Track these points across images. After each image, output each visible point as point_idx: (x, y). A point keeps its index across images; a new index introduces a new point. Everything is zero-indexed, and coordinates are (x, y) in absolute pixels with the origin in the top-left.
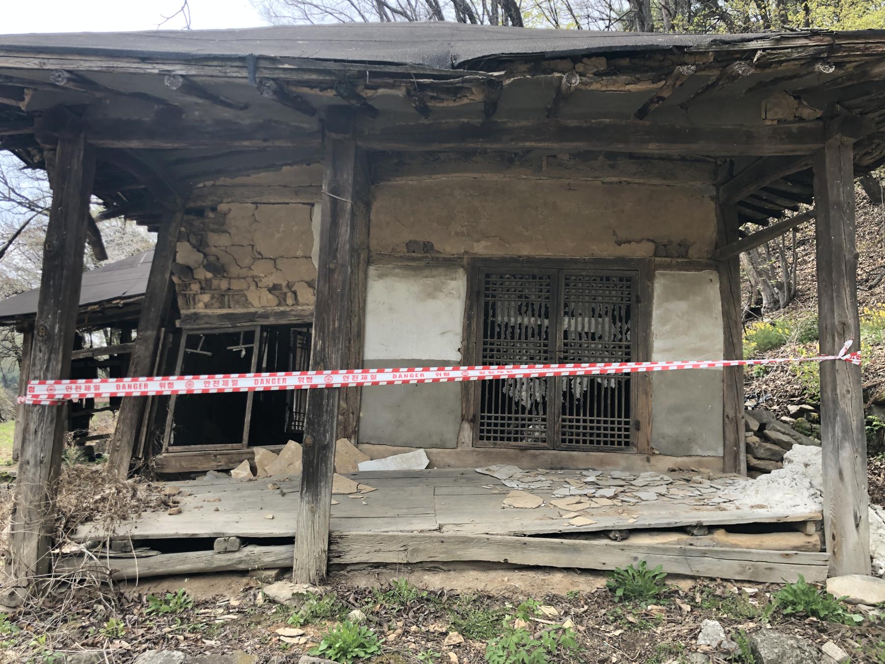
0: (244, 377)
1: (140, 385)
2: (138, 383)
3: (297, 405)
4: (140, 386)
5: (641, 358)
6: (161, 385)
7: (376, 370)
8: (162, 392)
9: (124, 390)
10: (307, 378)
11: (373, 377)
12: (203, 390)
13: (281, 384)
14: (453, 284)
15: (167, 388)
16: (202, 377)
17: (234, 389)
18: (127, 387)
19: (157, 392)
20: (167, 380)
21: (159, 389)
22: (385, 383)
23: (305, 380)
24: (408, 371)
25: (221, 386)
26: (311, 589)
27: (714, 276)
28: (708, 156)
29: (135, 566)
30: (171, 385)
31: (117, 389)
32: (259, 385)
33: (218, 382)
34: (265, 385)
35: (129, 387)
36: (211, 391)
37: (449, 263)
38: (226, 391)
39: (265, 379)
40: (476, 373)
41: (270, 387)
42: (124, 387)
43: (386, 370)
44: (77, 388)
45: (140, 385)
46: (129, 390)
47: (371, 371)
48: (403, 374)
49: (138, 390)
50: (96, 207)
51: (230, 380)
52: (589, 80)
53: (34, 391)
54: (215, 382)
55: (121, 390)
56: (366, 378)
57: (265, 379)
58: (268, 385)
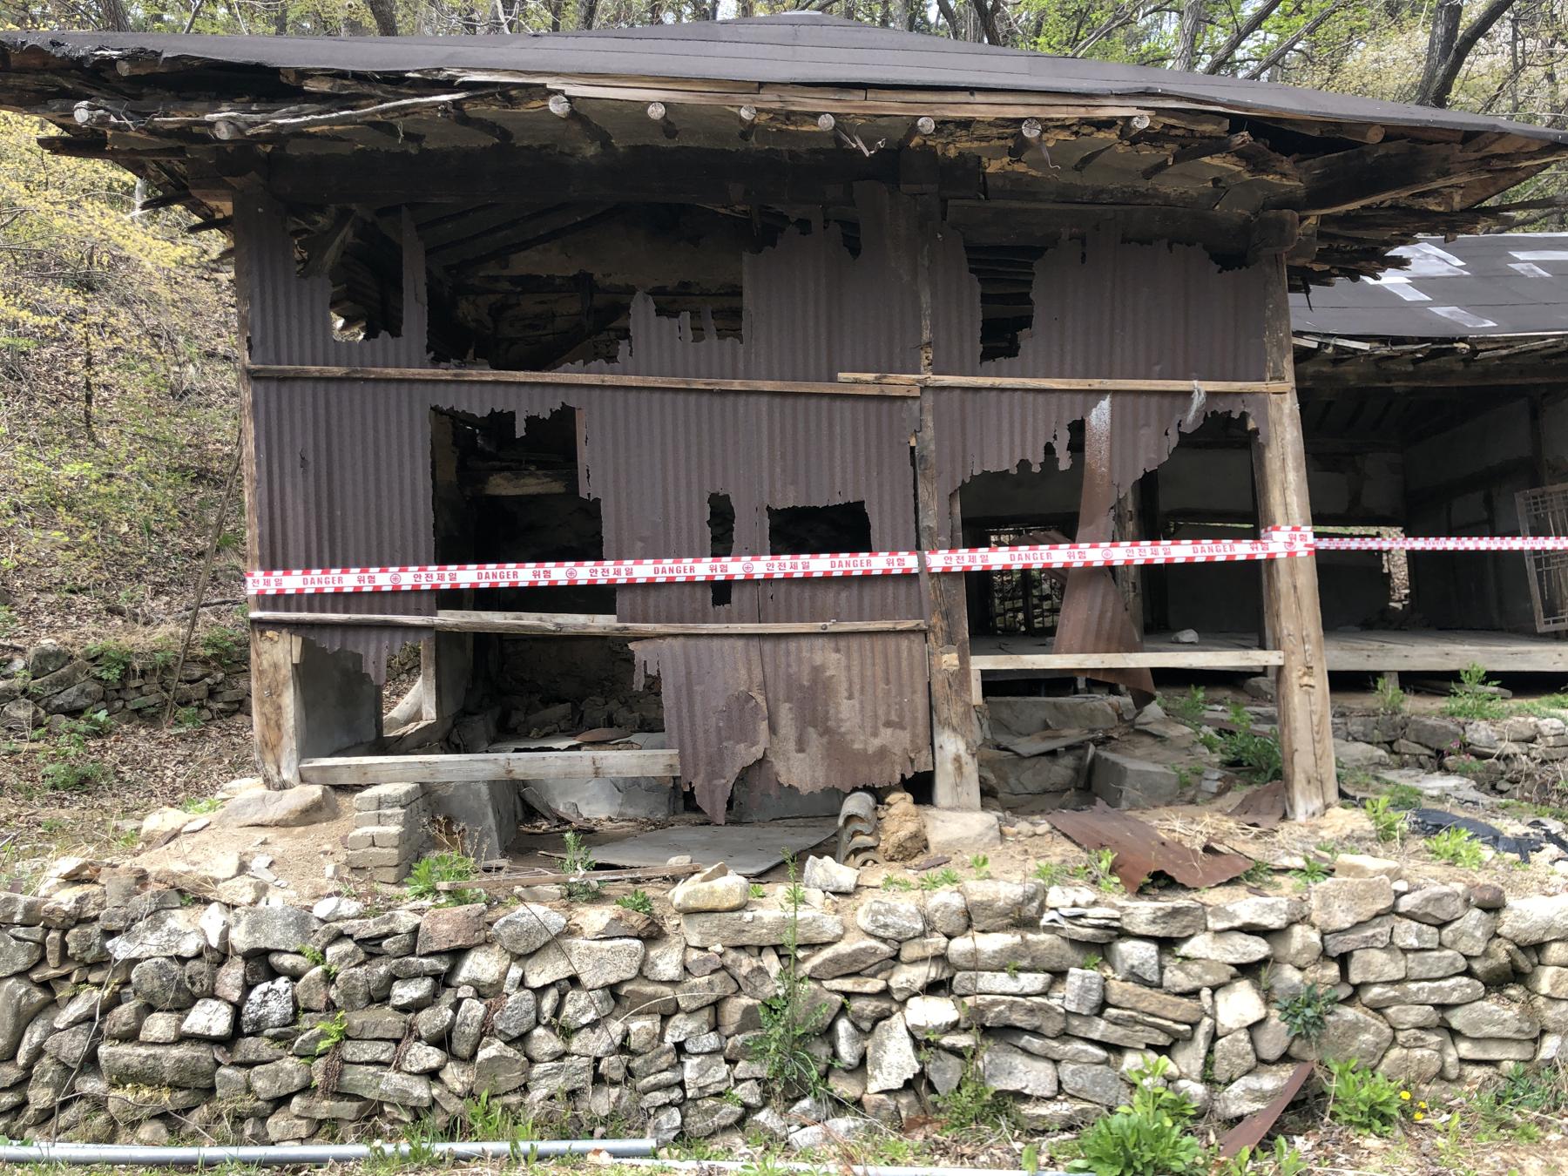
3: (378, 598)
5: (387, 558)
15: (367, 583)
16: (528, 565)
34: (1208, 554)
35: (319, 581)
38: (1156, 562)
39: (1206, 547)
42: (840, 564)
48: (1206, 547)
50: (1370, 281)
52: (774, 123)
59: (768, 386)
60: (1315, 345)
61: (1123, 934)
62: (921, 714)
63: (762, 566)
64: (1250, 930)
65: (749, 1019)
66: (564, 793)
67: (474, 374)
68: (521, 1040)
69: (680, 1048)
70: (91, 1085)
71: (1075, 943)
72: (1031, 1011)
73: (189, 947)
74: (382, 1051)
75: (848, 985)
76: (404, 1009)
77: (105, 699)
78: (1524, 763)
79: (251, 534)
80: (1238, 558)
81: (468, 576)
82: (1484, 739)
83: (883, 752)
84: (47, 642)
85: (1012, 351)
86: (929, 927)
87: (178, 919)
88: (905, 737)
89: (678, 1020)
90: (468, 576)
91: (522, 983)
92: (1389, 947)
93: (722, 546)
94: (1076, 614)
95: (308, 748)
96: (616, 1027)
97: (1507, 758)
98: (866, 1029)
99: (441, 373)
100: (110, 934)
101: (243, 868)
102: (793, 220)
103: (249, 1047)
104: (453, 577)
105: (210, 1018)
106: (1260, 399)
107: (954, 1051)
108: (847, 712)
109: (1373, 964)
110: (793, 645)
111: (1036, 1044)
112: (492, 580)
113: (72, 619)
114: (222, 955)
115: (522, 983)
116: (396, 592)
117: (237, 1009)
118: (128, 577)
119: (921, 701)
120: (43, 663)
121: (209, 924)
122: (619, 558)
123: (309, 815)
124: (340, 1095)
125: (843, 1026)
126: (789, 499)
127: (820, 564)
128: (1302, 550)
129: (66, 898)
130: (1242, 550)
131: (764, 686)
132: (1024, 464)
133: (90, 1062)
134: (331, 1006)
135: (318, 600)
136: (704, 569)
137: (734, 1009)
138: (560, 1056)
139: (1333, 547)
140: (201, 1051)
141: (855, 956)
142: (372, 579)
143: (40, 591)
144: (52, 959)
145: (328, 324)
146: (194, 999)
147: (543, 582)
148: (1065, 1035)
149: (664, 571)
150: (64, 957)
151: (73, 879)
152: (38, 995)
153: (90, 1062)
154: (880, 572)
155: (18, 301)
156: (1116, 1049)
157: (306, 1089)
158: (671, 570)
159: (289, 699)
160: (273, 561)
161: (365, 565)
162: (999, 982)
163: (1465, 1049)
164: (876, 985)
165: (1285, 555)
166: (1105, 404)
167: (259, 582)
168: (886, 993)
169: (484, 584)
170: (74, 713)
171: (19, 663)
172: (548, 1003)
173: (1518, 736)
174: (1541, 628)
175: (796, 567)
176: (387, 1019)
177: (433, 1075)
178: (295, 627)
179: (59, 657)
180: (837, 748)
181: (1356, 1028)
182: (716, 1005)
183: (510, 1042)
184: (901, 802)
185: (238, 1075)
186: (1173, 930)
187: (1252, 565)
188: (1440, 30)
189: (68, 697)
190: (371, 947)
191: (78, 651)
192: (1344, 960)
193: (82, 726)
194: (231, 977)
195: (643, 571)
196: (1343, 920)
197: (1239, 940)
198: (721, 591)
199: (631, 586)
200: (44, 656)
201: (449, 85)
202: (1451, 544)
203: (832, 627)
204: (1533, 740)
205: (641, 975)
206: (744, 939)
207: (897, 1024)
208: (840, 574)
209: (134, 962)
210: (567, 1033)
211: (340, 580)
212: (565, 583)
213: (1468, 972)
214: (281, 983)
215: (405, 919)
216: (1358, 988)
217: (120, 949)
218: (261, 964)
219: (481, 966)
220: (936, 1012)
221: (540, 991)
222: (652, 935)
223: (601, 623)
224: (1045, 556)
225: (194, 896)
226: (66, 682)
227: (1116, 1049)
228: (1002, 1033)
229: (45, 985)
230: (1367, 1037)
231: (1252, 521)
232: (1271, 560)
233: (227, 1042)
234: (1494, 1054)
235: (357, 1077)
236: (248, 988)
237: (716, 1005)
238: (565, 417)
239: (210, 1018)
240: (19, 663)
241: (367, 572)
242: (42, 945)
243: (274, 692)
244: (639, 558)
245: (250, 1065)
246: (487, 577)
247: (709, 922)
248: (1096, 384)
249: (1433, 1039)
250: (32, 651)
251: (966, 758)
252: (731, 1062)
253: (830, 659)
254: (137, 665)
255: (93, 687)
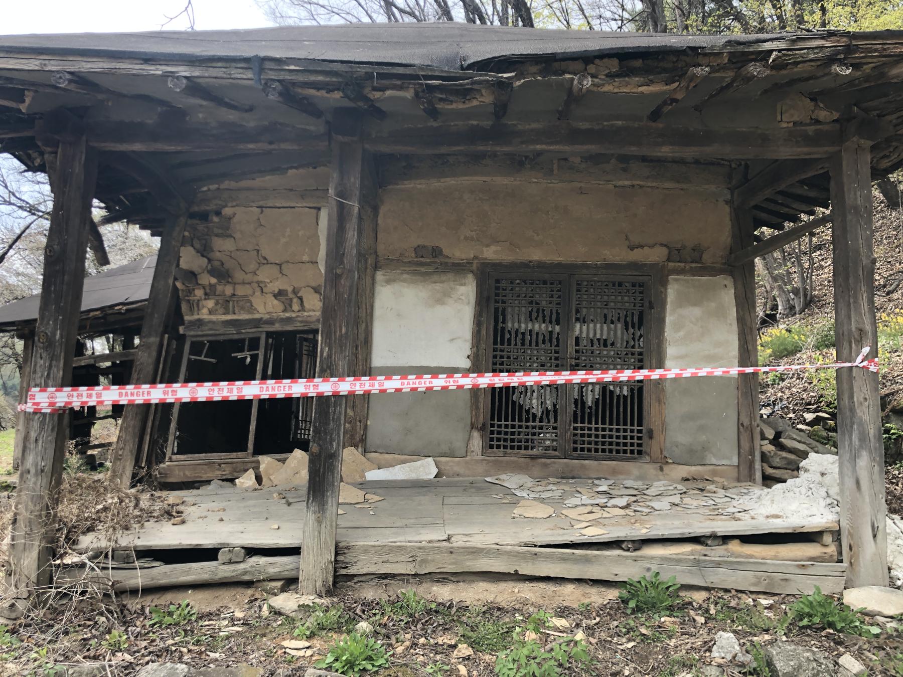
0: (249, 384)
1: (143, 392)
2: (141, 391)
4: (143, 394)
5: (654, 365)
6: (165, 393)
7: (383, 378)
8: (165, 399)
9: (127, 398)
10: (314, 385)
11: (381, 385)
12: (207, 397)
13: (287, 392)
14: (462, 289)
15: (170, 396)
16: (206, 384)
17: (239, 396)
18: (129, 394)
19: (160, 399)
20: (171, 387)
21: (162, 396)
22: (393, 391)
23: (312, 388)
24: (416, 379)
25: (225, 394)
26: (317, 601)
27: (729, 281)
28: (722, 159)
29: (138, 577)
30: (174, 392)
31: (120, 396)
32: (264, 393)
33: (223, 389)
34: (271, 392)
35: (132, 394)
36: (215, 399)
37: (458, 268)
38: (231, 398)
39: (270, 386)
40: (486, 380)
41: (276, 395)
42: (126, 394)
43: (394, 377)
44: (78, 395)
45: (143, 392)
46: (132, 398)
47: (379, 378)
48: (411, 382)
49: (141, 397)
51: (235, 388)
53: (34, 399)
54: (219, 389)
55: (123, 398)
56: (373, 385)
57: (270, 386)
58: (273, 393)
102: (613, 161)
145: (89, 207)
187: (638, 389)
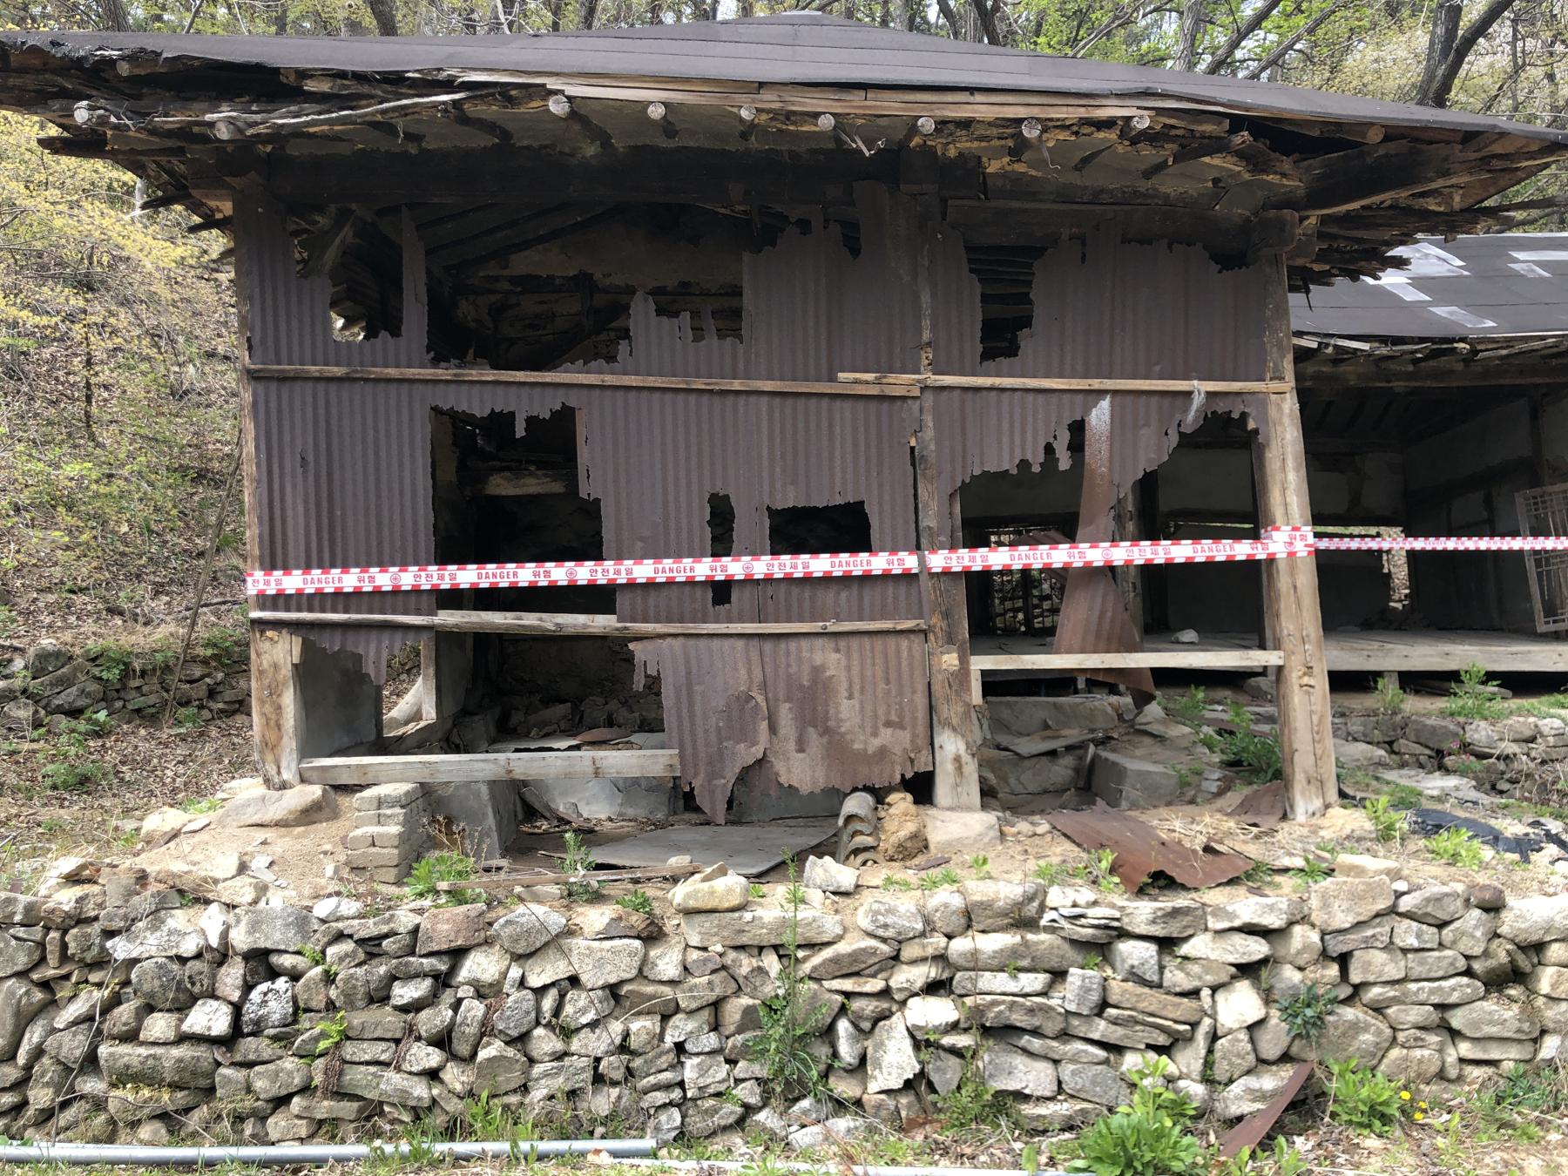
3: (378, 598)
5: (387, 558)
15: (367, 583)
16: (528, 565)
34: (1208, 554)
35: (319, 581)
38: (1156, 562)
39: (1206, 547)
42: (840, 564)
48: (1206, 547)
59: (768, 386)
60: (1315, 345)
61: (1123, 934)
62: (921, 714)
63: (762, 566)
64: (1250, 930)
65: (749, 1019)
66: (564, 793)
67: (474, 374)
68: (521, 1040)
69: (680, 1048)
70: (91, 1085)
71: (1075, 943)
72: (1031, 1011)
73: (189, 947)
74: (382, 1051)
75: (848, 985)
76: (404, 1009)
77: (105, 699)
78: (1524, 763)
79: (251, 534)
80: (1238, 558)
81: (468, 576)
82: (1484, 739)
83: (883, 752)
84: (47, 642)
85: (1012, 351)
86: (929, 927)
87: (178, 919)
88: (905, 737)
89: (678, 1020)
90: (468, 576)
91: (522, 983)
92: (1389, 947)
93: (722, 546)
94: (1076, 614)
95: (308, 748)
96: (616, 1027)
97: (1507, 758)
98: (866, 1029)
99: (441, 373)
100: (110, 934)
101: (243, 868)
102: (793, 220)
103: (249, 1047)
104: (453, 577)
105: (210, 1018)
106: (1260, 399)
107: (954, 1051)
108: (847, 712)
109: (1373, 964)
110: (793, 645)
111: (1036, 1044)
112: (492, 580)
113: (72, 619)
114: (222, 955)
115: (522, 983)
116: (396, 592)
117: (237, 1009)
118: (128, 577)
119: (921, 701)
120: (43, 663)
121: (209, 924)
122: (619, 558)
123: (309, 815)
124: (340, 1095)
125: (843, 1026)
126: (789, 499)
127: (820, 564)
128: (1302, 550)
129: (66, 898)
130: (1242, 550)
131: (764, 686)
132: (1024, 464)
133: (90, 1062)
134: (331, 1006)
135: (318, 600)
136: (704, 569)
137: (734, 1009)
138: (560, 1056)
139: (1333, 547)
140: (201, 1051)
141: (855, 956)
142: (372, 579)
143: (40, 591)
144: (52, 959)
145: (328, 324)
146: (194, 999)
147: (543, 582)
148: (1065, 1035)
149: (664, 571)
150: (64, 957)
151: (73, 879)
152: (38, 995)
153: (90, 1062)
154: (880, 572)
155: (18, 301)
156: (1116, 1049)
157: (306, 1089)
158: (671, 570)
159: (289, 699)
160: (273, 561)
161: (365, 565)
162: (999, 982)
163: (1465, 1049)
164: (876, 985)
165: (1285, 555)
166: (1105, 404)
167: (259, 582)
168: (886, 993)
169: (484, 584)
170: (74, 713)
171: (19, 663)
172: (548, 1003)
173: (1518, 736)
174: (1541, 628)
175: (796, 567)
176: (387, 1019)
177: (433, 1075)
178: (295, 627)
179: (59, 657)
180: (837, 748)
181: (1356, 1028)
182: (716, 1005)
183: (510, 1042)
184: (901, 802)
185: (238, 1075)
186: (1173, 930)
187: (1252, 565)
188: (1440, 30)
189: (68, 697)
190: (371, 947)
191: (78, 651)
192: (1344, 960)
193: (82, 726)
194: (231, 977)
195: (643, 571)
196: (1343, 920)
197: (1239, 940)
198: (721, 591)
199: (631, 586)
200: (44, 656)
201: (449, 85)
202: (1451, 544)
203: (832, 627)
204: (1533, 740)
205: (641, 975)
206: (744, 939)
207: (897, 1024)
208: (840, 574)
209: (134, 962)
210: (567, 1033)
211: (340, 580)
212: (565, 583)
213: (1468, 972)
214: (281, 983)
215: (405, 919)
216: (1358, 988)
217: (120, 949)
218: (261, 964)
219: (481, 966)
220: (936, 1012)
221: (540, 991)
222: (652, 935)
223: (601, 623)
224: (1045, 556)
225: (194, 896)
226: (66, 682)
227: (1116, 1049)
228: (1002, 1033)
229: (45, 985)
230: (1367, 1037)
231: (1252, 521)
232: (1271, 560)
233: (227, 1042)
234: (1494, 1054)
235: (357, 1077)
236: (248, 988)
237: (716, 1005)
238: (565, 417)
239: (210, 1018)
240: (19, 663)
241: (367, 572)
242: (42, 945)
243: (274, 692)
244: (639, 558)
245: (250, 1065)
246: (487, 577)
247: (709, 922)
248: (1096, 384)
249: (1433, 1039)
250: (32, 651)
251: (966, 758)
252: (731, 1062)
253: (830, 659)
254: (137, 665)
255: (93, 687)
